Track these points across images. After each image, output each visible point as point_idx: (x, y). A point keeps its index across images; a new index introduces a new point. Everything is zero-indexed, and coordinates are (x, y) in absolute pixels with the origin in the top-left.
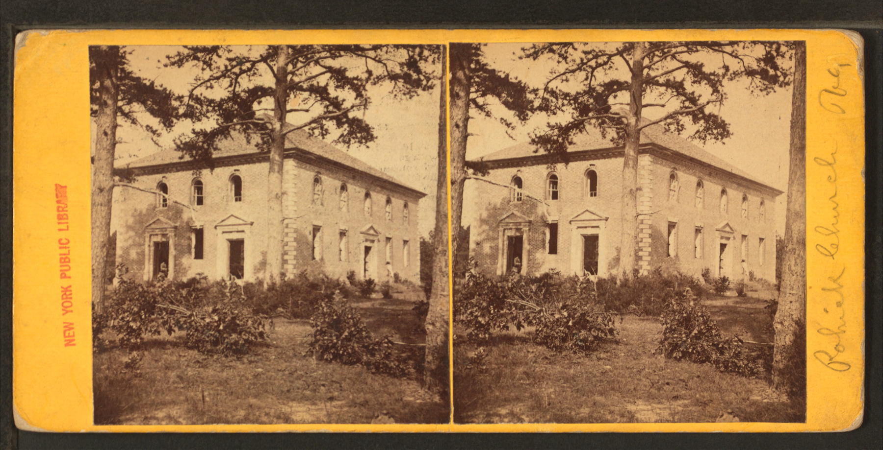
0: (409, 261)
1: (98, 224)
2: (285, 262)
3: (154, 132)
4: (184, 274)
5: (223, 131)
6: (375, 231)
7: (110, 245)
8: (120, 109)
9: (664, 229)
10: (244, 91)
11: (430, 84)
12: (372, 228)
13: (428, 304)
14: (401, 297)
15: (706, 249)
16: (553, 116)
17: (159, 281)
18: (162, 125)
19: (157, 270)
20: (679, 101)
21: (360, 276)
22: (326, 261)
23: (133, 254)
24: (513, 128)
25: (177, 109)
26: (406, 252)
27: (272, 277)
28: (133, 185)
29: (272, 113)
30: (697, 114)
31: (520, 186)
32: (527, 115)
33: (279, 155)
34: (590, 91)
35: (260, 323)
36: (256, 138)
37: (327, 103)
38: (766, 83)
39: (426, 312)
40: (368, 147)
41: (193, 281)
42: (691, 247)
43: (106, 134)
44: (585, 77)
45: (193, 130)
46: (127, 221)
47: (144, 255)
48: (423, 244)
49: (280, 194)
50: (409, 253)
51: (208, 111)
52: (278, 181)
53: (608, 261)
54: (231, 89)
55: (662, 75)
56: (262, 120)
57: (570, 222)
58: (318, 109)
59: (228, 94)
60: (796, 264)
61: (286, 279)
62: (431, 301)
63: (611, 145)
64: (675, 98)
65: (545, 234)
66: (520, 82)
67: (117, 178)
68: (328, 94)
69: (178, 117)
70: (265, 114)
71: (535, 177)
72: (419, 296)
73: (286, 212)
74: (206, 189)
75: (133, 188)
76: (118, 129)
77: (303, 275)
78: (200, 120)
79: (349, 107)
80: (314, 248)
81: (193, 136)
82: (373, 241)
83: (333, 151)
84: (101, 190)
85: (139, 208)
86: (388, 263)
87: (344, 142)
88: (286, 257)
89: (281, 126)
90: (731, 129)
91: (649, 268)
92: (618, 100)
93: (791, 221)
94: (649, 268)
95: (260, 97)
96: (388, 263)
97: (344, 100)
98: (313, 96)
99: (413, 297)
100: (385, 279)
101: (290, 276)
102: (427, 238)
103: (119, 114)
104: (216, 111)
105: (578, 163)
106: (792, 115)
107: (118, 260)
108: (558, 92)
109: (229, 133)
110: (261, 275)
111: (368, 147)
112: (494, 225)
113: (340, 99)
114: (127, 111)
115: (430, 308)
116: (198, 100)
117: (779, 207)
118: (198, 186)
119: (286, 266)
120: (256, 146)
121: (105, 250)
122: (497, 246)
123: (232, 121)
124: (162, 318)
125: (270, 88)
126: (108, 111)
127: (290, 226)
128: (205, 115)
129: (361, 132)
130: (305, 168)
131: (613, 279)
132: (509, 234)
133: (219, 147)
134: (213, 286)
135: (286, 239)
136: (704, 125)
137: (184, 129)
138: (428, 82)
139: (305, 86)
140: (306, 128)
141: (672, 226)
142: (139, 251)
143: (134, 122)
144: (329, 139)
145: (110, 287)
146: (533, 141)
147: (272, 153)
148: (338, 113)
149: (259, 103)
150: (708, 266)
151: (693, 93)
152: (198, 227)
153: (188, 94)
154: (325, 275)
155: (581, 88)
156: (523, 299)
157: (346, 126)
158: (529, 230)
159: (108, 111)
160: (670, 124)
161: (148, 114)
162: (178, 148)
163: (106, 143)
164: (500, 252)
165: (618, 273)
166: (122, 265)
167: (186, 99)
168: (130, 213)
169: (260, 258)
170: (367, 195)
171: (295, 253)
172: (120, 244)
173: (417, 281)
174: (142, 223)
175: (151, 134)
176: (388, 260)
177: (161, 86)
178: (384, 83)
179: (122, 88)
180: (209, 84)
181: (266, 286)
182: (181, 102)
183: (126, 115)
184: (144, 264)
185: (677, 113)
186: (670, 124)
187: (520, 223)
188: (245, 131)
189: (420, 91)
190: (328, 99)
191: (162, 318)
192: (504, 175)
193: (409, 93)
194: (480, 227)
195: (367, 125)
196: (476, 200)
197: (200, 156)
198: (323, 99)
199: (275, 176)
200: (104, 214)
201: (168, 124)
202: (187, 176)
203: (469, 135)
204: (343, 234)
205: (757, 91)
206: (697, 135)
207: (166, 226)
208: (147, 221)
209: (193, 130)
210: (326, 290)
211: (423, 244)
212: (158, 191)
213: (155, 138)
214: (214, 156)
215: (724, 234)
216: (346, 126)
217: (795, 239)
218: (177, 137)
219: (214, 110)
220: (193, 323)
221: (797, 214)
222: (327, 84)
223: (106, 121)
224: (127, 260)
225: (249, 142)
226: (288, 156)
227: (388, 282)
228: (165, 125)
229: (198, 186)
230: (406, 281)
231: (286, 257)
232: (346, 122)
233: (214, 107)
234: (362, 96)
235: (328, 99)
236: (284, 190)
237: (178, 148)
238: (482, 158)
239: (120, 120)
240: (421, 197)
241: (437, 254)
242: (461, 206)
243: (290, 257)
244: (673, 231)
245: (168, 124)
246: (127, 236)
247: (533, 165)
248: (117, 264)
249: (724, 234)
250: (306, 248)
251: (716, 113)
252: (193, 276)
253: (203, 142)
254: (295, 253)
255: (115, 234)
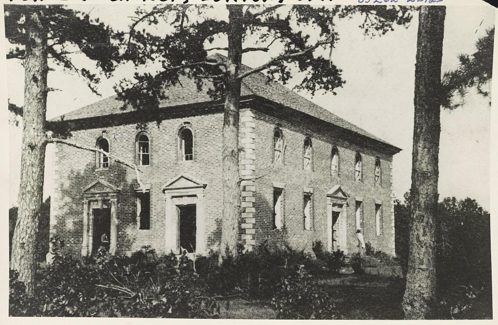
0: (382, 228)
1: (29, 188)
2: (242, 231)
3: (91, 77)
4: (129, 247)
5: (170, 76)
6: (344, 194)
7: (43, 214)
8: (50, 49)
9: (269, 197)
10: (193, 26)
11: (406, 15)
12: (340, 190)
13: (405, 279)
14: (374, 272)
15: (318, 218)
16: (141, 66)
17: (99, 256)
18: (100, 68)
19: (97, 242)
20: (284, 43)
21: (329, 248)
22: (289, 230)
23: (70, 225)
24: (97, 81)
25: (116, 49)
26: (378, 218)
27: (227, 249)
28: (68, 141)
29: (225, 53)
30: (305, 59)
31: (106, 149)
32: (112, 64)
33: (235, 104)
34: (182, 33)
35: (215, 306)
36: (208, 84)
37: (289, 40)
38: (382, 19)
39: (403, 289)
40: (335, 94)
41: (139, 255)
42: (300, 217)
43: (35, 79)
44: (175, 17)
45: (136, 74)
46: (62, 185)
47: (82, 225)
48: (398, 208)
49: (236, 150)
50: (381, 219)
51: (152, 52)
52: (233, 135)
53: (206, 237)
54: (177, 24)
55: (264, 12)
56: (215, 61)
57: (164, 191)
58: (278, 48)
59: (174, 30)
60: (424, 234)
61: (244, 252)
62: (408, 276)
63: (208, 99)
64: (280, 39)
65: (136, 206)
66: (102, 24)
67: (50, 133)
68: (290, 29)
69: (119, 59)
70: (218, 55)
71: (123, 138)
72: (394, 271)
73: (243, 173)
74: (153, 144)
75: (70, 145)
76: (50, 73)
77: (262, 248)
78: (143, 63)
79: (314, 45)
80: (274, 214)
81: (136, 81)
82: (341, 206)
83: (296, 99)
84: (32, 147)
85: (76, 169)
86: (359, 231)
87: (308, 87)
88: (243, 226)
89: (237, 69)
90: (343, 76)
91: (253, 242)
92: (214, 44)
93: (417, 183)
94: (253, 242)
95: (213, 33)
96: (359, 231)
97: (308, 36)
98: (273, 31)
99: (385, 271)
100: (356, 250)
101: (248, 248)
102: (403, 201)
103: (50, 55)
104: (161, 51)
105: (171, 121)
106: (417, 57)
107: (53, 231)
108: (146, 36)
109: (177, 79)
110: (215, 248)
111: (335, 94)
112: (77, 197)
113: (303, 35)
114: (59, 52)
115: (408, 285)
116: (139, 37)
117: (401, 170)
118: (143, 141)
119: (244, 237)
120: (208, 93)
121: (36, 220)
122: (82, 221)
123: (180, 63)
124: (103, 301)
125: (223, 22)
126: (37, 52)
127: (247, 188)
128: (149, 57)
129: (327, 75)
130: (264, 120)
131: (215, 256)
132: (95, 207)
133: (166, 94)
134: (161, 260)
135: (243, 205)
136: (312, 72)
137: (126, 73)
138: (404, 13)
139: (263, 19)
140: (265, 72)
141: (277, 192)
142: (76, 220)
143: (68, 65)
144: (291, 84)
145: (42, 265)
146: (120, 94)
147: (227, 102)
148: (301, 53)
149: (211, 40)
150: (321, 239)
151: (300, 33)
152: (144, 191)
153: (128, 30)
154: (287, 246)
155: (171, 30)
156: (117, 284)
157: (310, 68)
158: (118, 201)
159: (37, 52)
160: (272, 72)
161: (84, 55)
162: (120, 97)
163: (36, 89)
164: (85, 228)
165: (219, 248)
166: (56, 237)
167: (127, 37)
168: (66, 175)
169: (214, 228)
170: (335, 151)
171: (254, 221)
172: (55, 213)
173: (391, 250)
174: (80, 187)
175: (88, 80)
176: (359, 228)
177: (97, 21)
178: (354, 15)
179: (52, 23)
180: (152, 18)
181: (221, 260)
182: (121, 40)
183: (58, 57)
184: (82, 236)
185: (282, 58)
186: (272, 72)
187: (107, 193)
188: (195, 74)
189: (394, 25)
190: (290, 35)
191: (103, 301)
192: (86, 137)
193: (382, 27)
194: (62, 199)
195: (334, 67)
196: (57, 168)
197: (144, 106)
198: (284, 35)
199: (230, 130)
200: (36, 176)
201: (108, 69)
202: (130, 130)
203: (49, 90)
204: (307, 197)
205: (372, 30)
206: (304, 85)
207: (108, 190)
208: (87, 184)
209: (136, 74)
210: (289, 265)
211: (398, 208)
212: (97, 149)
213: (93, 85)
214: (160, 106)
215: (335, 201)
216: (310, 68)
217: (422, 205)
218: (118, 83)
219: (159, 51)
220: (138, 307)
221: (424, 175)
222: (289, 18)
223: (35, 63)
224: (62, 231)
225: (199, 88)
226: (244, 106)
227: (359, 254)
228: (104, 69)
229: (143, 141)
230: (379, 253)
231: (243, 226)
232: (310, 64)
233: (159, 46)
234: (328, 31)
235: (290, 35)
236: (241, 145)
237: (120, 97)
238: (63, 117)
239: (51, 62)
240: (395, 153)
241: (413, 220)
242: (43, 175)
243: (248, 226)
244: (280, 198)
245: (108, 69)
246: (62, 203)
247: (120, 124)
248: (51, 236)
249: (335, 201)
250: (264, 214)
251: (326, 58)
252: (139, 249)
253: (148, 89)
254: (254, 221)
255: (49, 200)
